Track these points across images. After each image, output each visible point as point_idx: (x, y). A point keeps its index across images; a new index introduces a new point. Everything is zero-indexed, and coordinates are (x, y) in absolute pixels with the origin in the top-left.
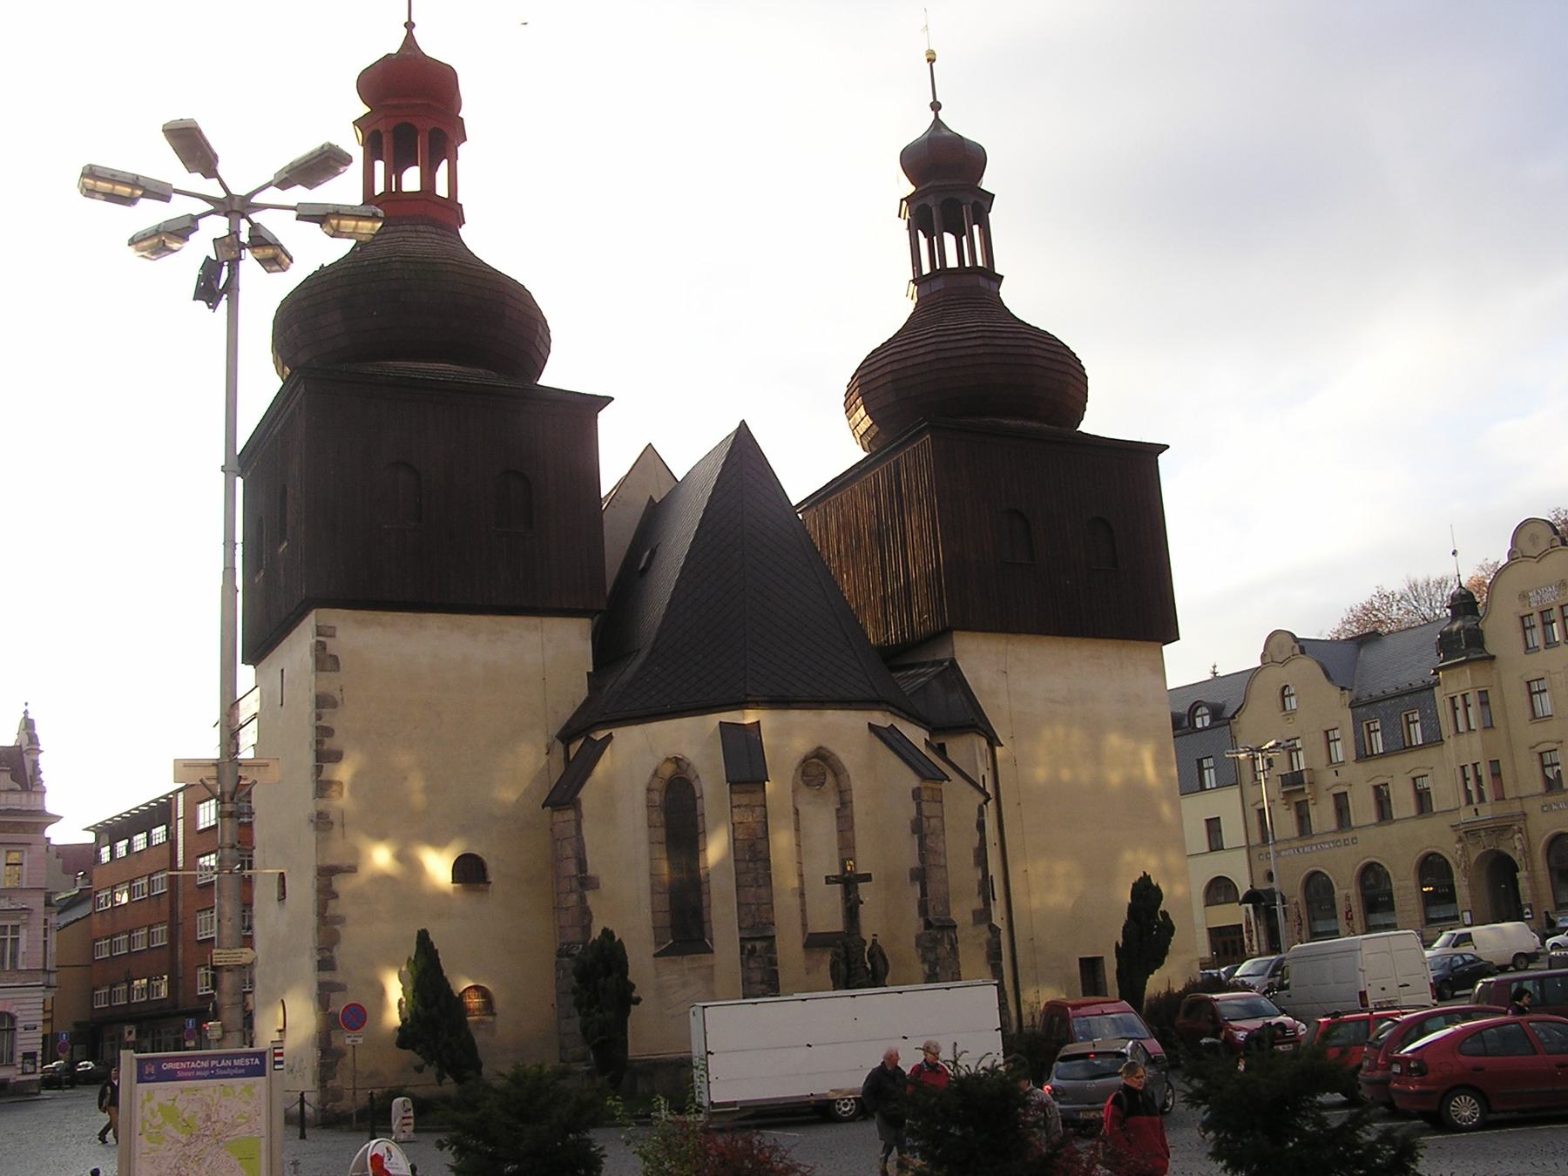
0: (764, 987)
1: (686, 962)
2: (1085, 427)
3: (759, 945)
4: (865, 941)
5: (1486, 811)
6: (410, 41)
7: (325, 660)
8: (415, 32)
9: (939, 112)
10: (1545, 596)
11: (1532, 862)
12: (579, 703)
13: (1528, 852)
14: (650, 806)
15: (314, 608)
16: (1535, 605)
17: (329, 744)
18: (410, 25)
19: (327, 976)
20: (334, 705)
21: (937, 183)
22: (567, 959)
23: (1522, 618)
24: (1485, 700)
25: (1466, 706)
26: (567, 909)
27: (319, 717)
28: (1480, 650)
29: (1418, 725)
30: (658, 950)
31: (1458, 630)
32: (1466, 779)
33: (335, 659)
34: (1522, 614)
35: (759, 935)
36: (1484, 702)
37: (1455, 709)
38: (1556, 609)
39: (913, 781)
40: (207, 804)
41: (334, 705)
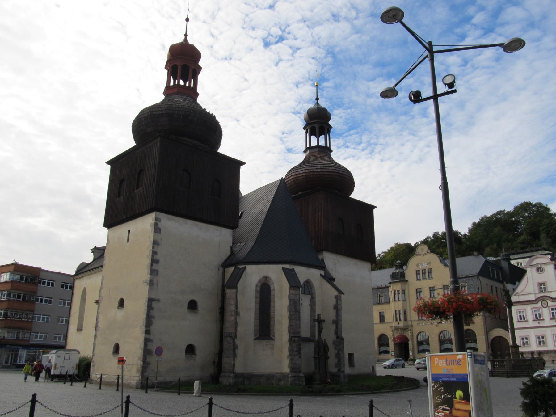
0: (297, 353)
1: (264, 342)
2: (353, 196)
3: (296, 339)
4: (323, 341)
5: (402, 324)
6: (186, 40)
7: (157, 229)
8: (188, 38)
9: (318, 101)
10: (424, 266)
11: (413, 339)
12: (228, 255)
13: (412, 336)
14: (256, 291)
15: (155, 211)
16: (421, 268)
17: (156, 257)
18: (186, 35)
19: (148, 336)
20: (158, 244)
21: (319, 121)
22: (229, 338)
23: (417, 271)
24: (404, 292)
25: (398, 294)
26: (230, 321)
27: (153, 247)
28: (403, 278)
29: (383, 298)
30: (255, 338)
31: (398, 273)
32: (396, 314)
33: (160, 229)
34: (417, 270)
35: (297, 336)
36: (404, 293)
37: (395, 294)
38: (427, 270)
39: (336, 293)
40: (6, 274)
41: (158, 244)
